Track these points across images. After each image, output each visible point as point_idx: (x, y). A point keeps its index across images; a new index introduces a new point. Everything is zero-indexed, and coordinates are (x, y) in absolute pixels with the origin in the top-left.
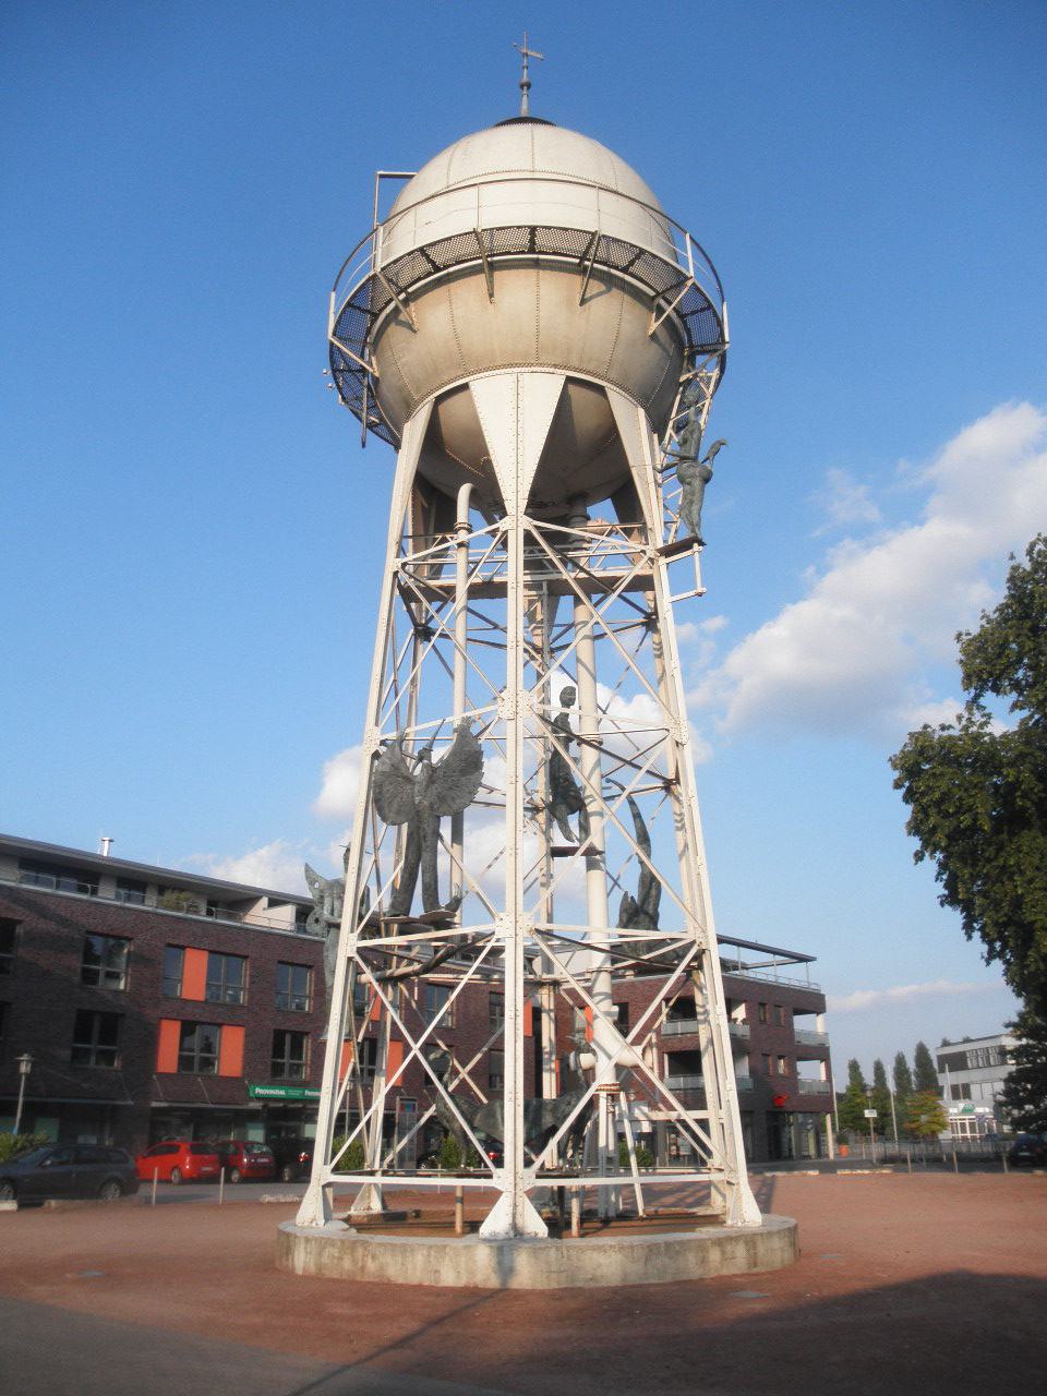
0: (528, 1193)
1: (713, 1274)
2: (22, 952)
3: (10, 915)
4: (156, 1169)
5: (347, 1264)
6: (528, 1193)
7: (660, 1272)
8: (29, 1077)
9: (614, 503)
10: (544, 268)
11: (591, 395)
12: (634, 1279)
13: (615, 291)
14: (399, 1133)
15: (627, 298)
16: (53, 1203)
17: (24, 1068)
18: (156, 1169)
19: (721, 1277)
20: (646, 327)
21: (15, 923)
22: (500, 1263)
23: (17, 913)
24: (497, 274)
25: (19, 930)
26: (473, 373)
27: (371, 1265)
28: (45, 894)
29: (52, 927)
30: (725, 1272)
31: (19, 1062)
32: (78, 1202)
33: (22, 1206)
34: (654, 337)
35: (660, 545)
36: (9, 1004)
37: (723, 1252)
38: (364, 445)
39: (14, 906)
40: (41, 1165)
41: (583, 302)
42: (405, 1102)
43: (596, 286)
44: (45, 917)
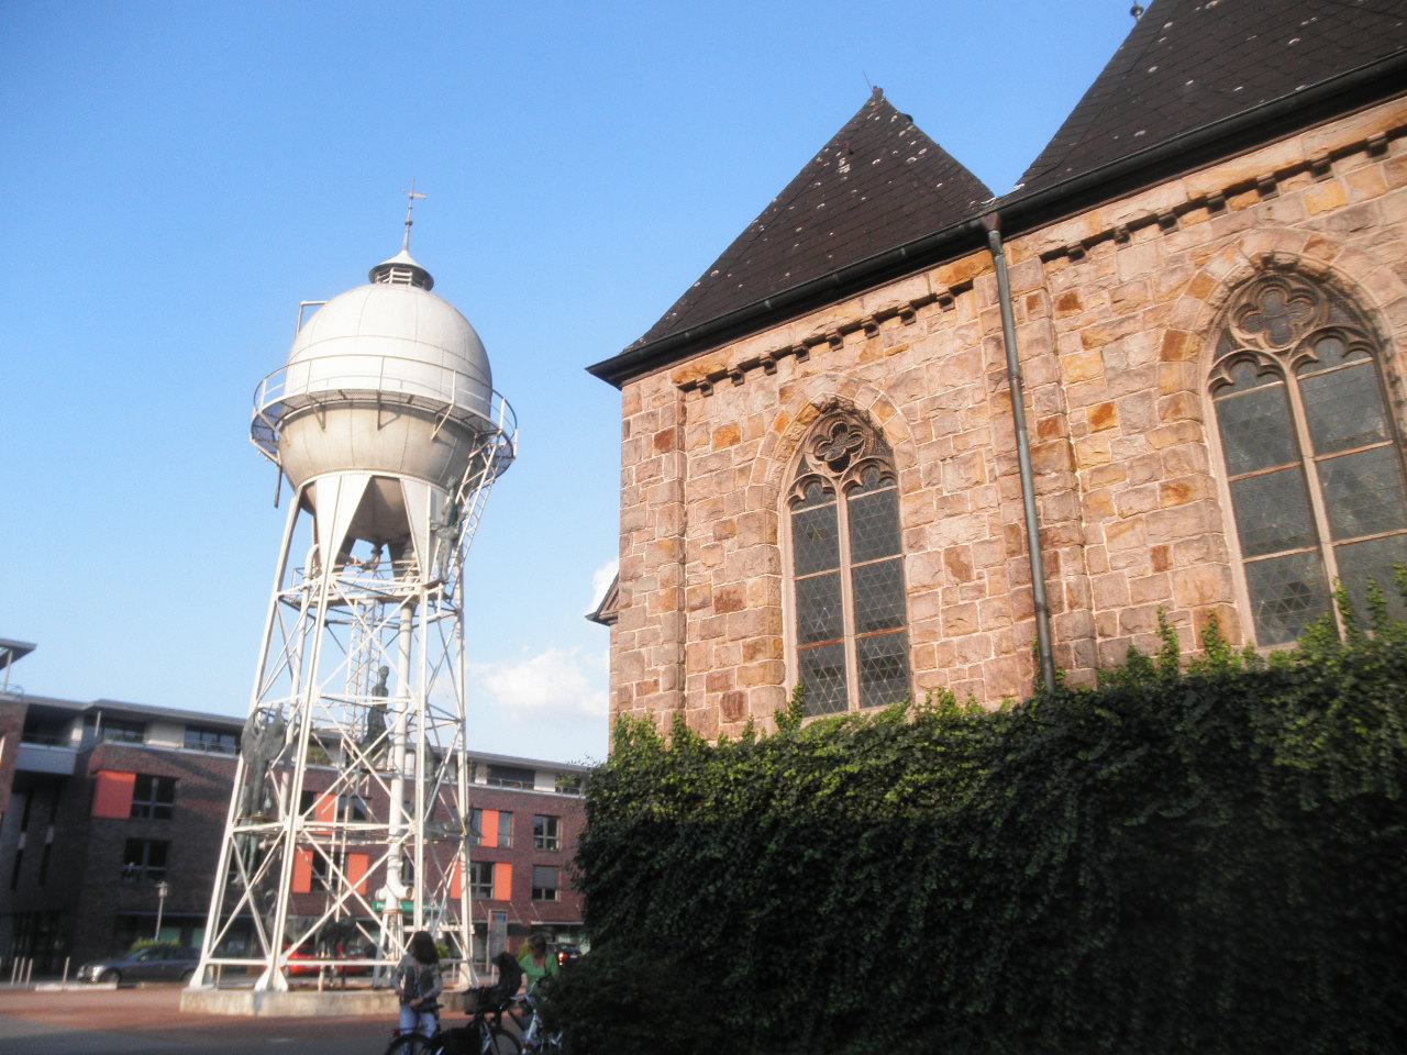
0: (283, 969)
1: (373, 1012)
2: (180, 803)
3: (170, 774)
4: (68, 960)
5: (194, 1005)
6: (283, 969)
7: (332, 1011)
8: (165, 899)
9: (1134, 32)
10: (356, 408)
11: (391, 483)
12: (322, 1013)
13: (403, 417)
14: (491, 939)
15: (413, 419)
16: (143, 985)
17: (162, 893)
18: (68, 960)
19: (378, 1015)
20: (430, 434)
21: (174, 780)
22: (255, 1003)
23: (176, 772)
24: (328, 413)
25: (178, 785)
26: (318, 474)
27: (202, 1005)
28: (198, 757)
29: (204, 781)
30: (381, 1012)
31: (159, 889)
32: (161, 985)
33: (119, 988)
34: (436, 439)
35: (426, 582)
36: (171, 841)
37: (382, 1001)
38: (277, 506)
39: (171, 766)
40: (139, 960)
41: (380, 427)
42: (496, 914)
43: (387, 416)
44: (198, 774)
